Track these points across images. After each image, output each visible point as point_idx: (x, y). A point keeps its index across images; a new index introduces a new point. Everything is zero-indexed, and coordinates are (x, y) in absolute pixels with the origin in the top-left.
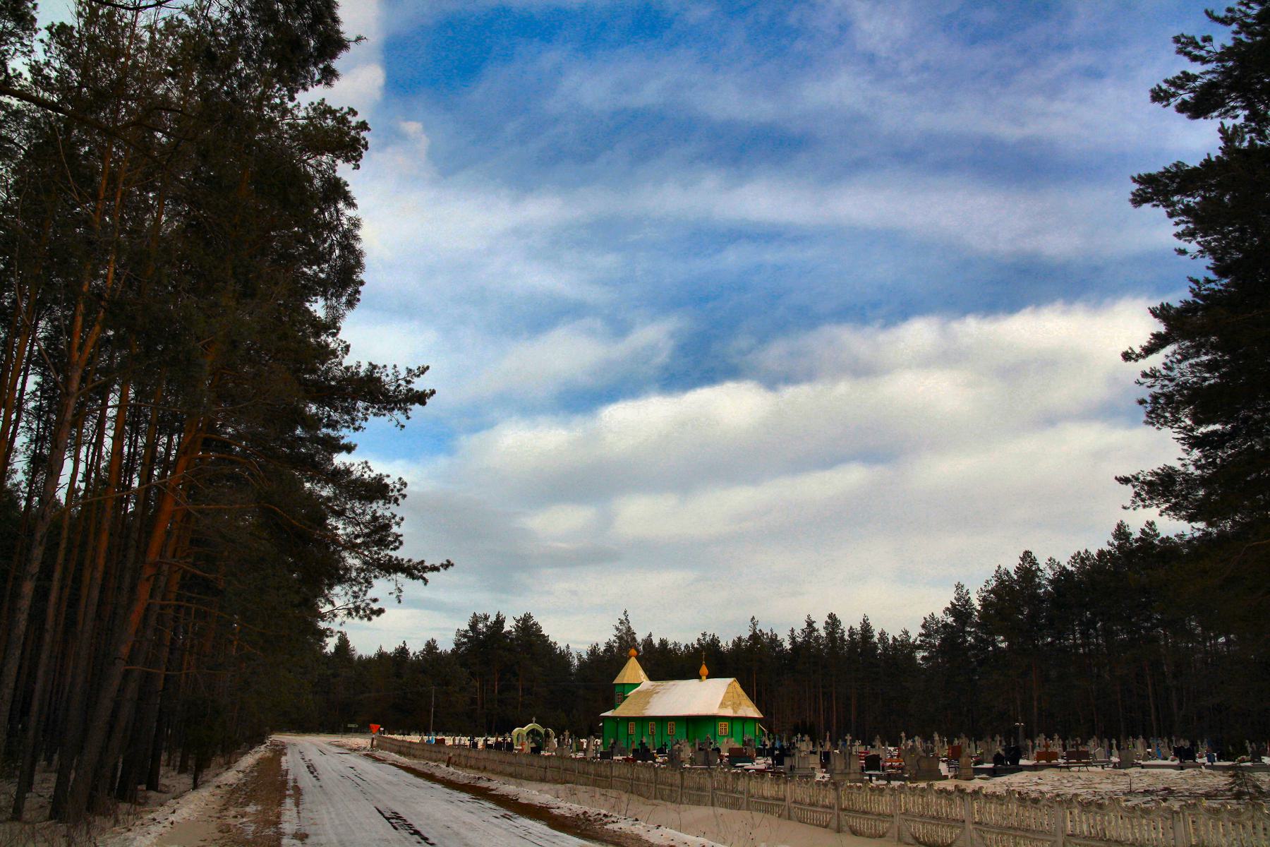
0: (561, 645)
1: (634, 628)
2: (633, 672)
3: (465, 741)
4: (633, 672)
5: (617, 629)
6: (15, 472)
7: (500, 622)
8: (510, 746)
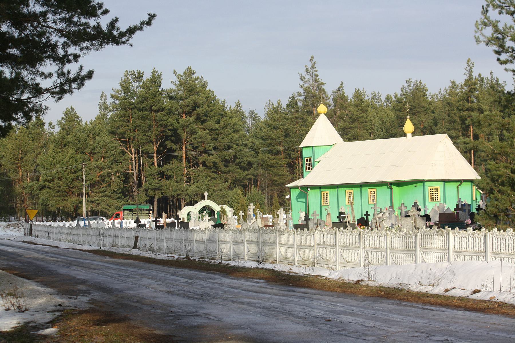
0: (230, 105)
1: (322, 78)
2: (322, 133)
3: (130, 223)
4: (322, 133)
5: (302, 79)
6: (56, 42)
7: (156, 80)
8: (185, 225)
